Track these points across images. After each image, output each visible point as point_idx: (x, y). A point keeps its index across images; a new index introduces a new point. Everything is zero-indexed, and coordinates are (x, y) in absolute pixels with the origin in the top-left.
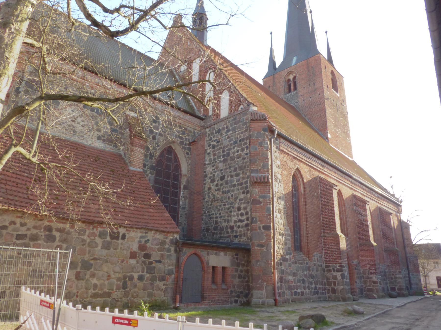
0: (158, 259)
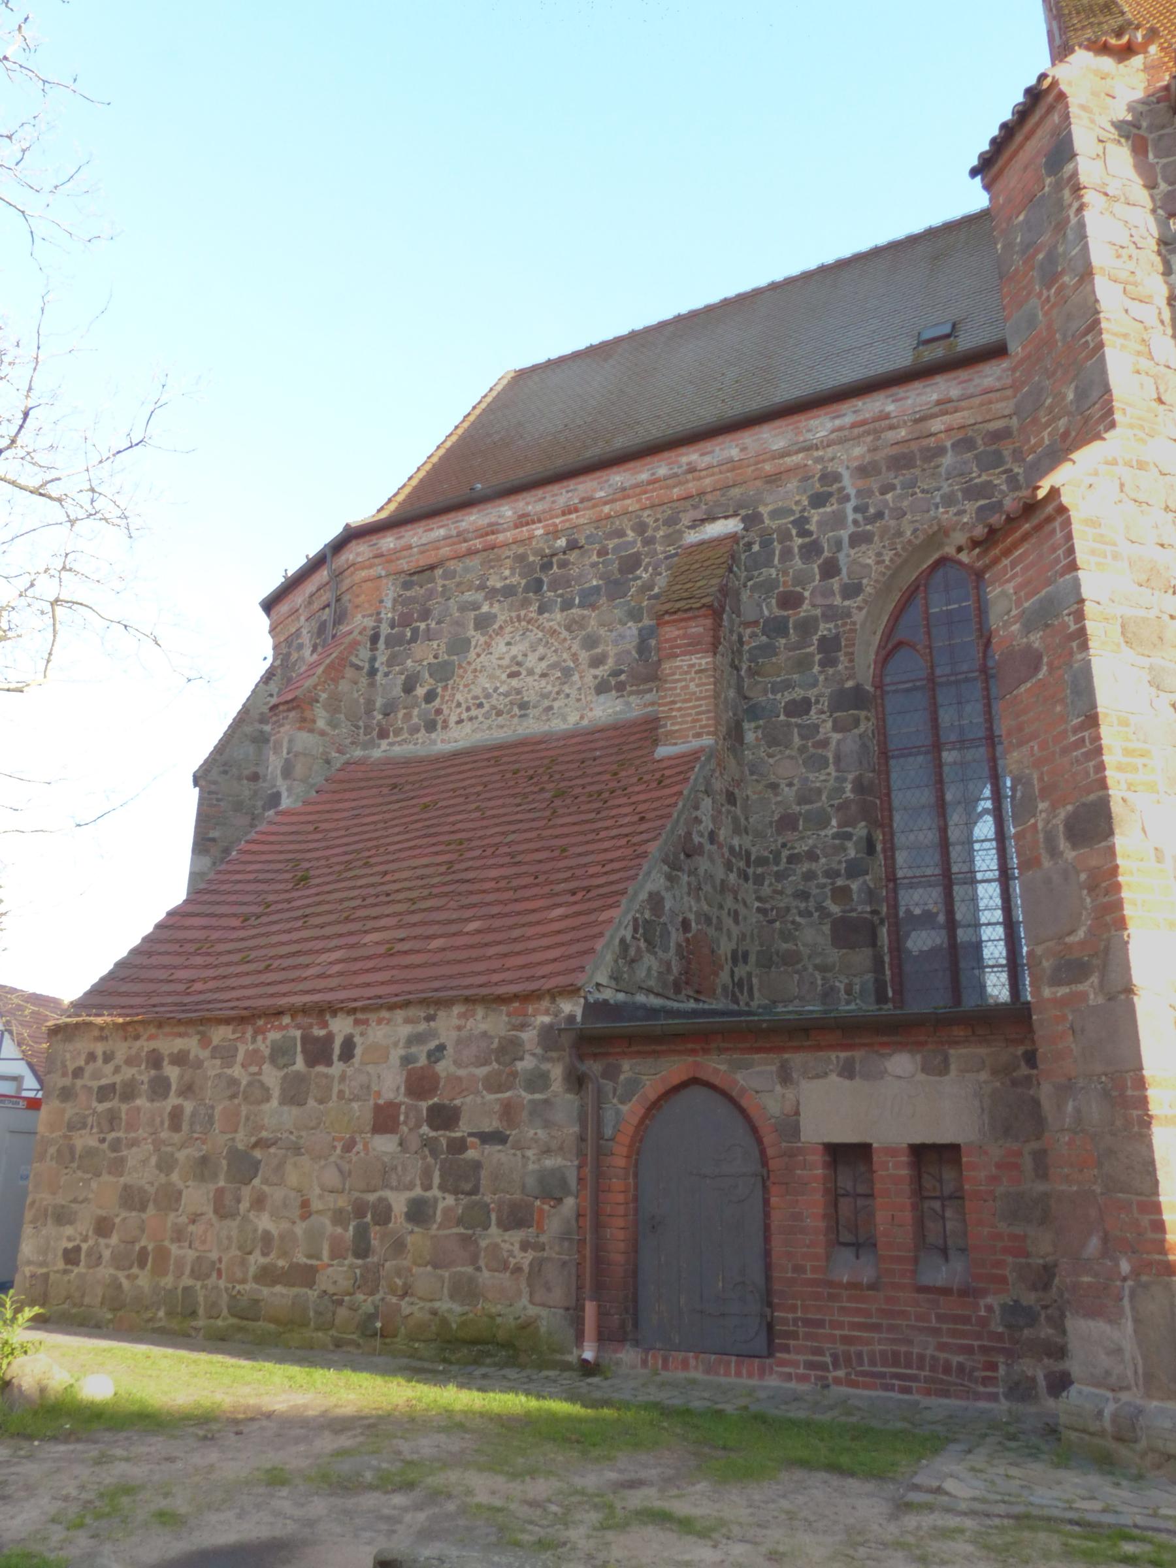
0: (491, 1124)
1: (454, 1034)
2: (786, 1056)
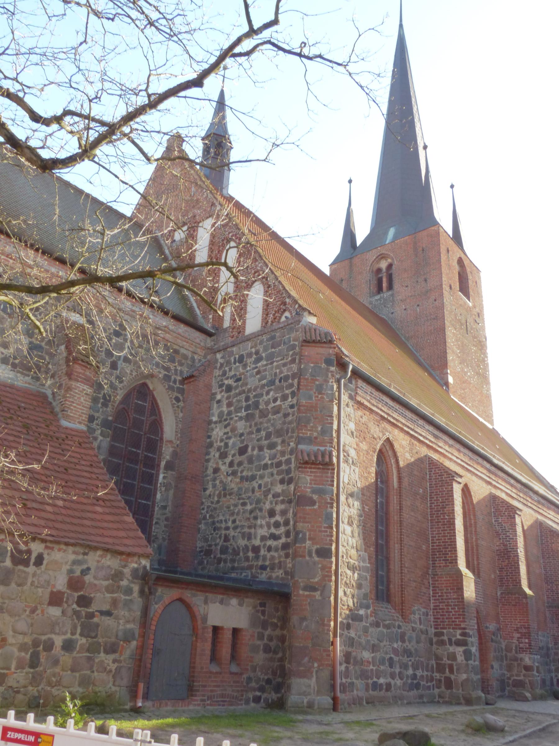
0: (106, 607)
1: (95, 563)
2: (207, 594)
